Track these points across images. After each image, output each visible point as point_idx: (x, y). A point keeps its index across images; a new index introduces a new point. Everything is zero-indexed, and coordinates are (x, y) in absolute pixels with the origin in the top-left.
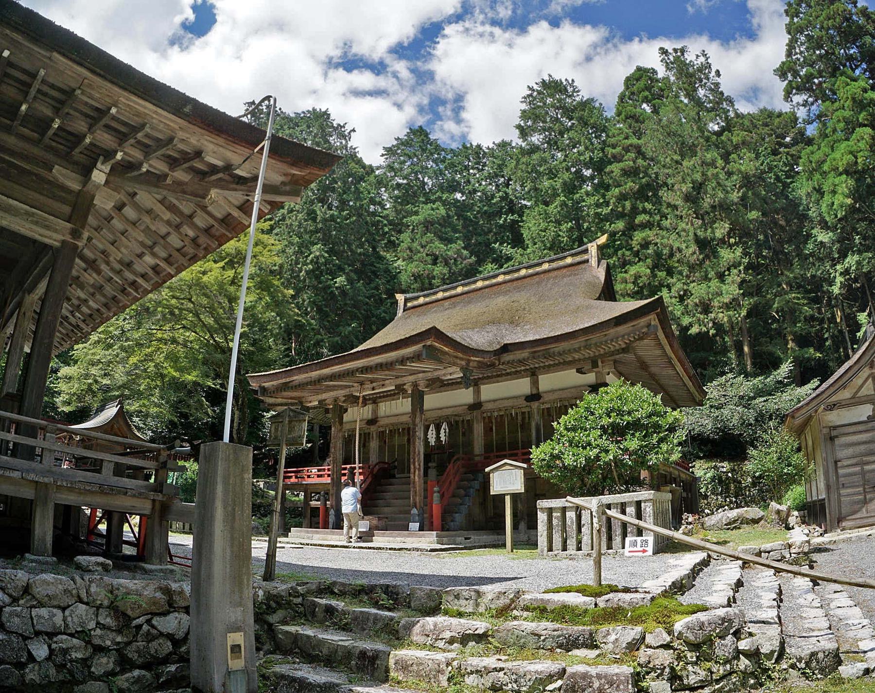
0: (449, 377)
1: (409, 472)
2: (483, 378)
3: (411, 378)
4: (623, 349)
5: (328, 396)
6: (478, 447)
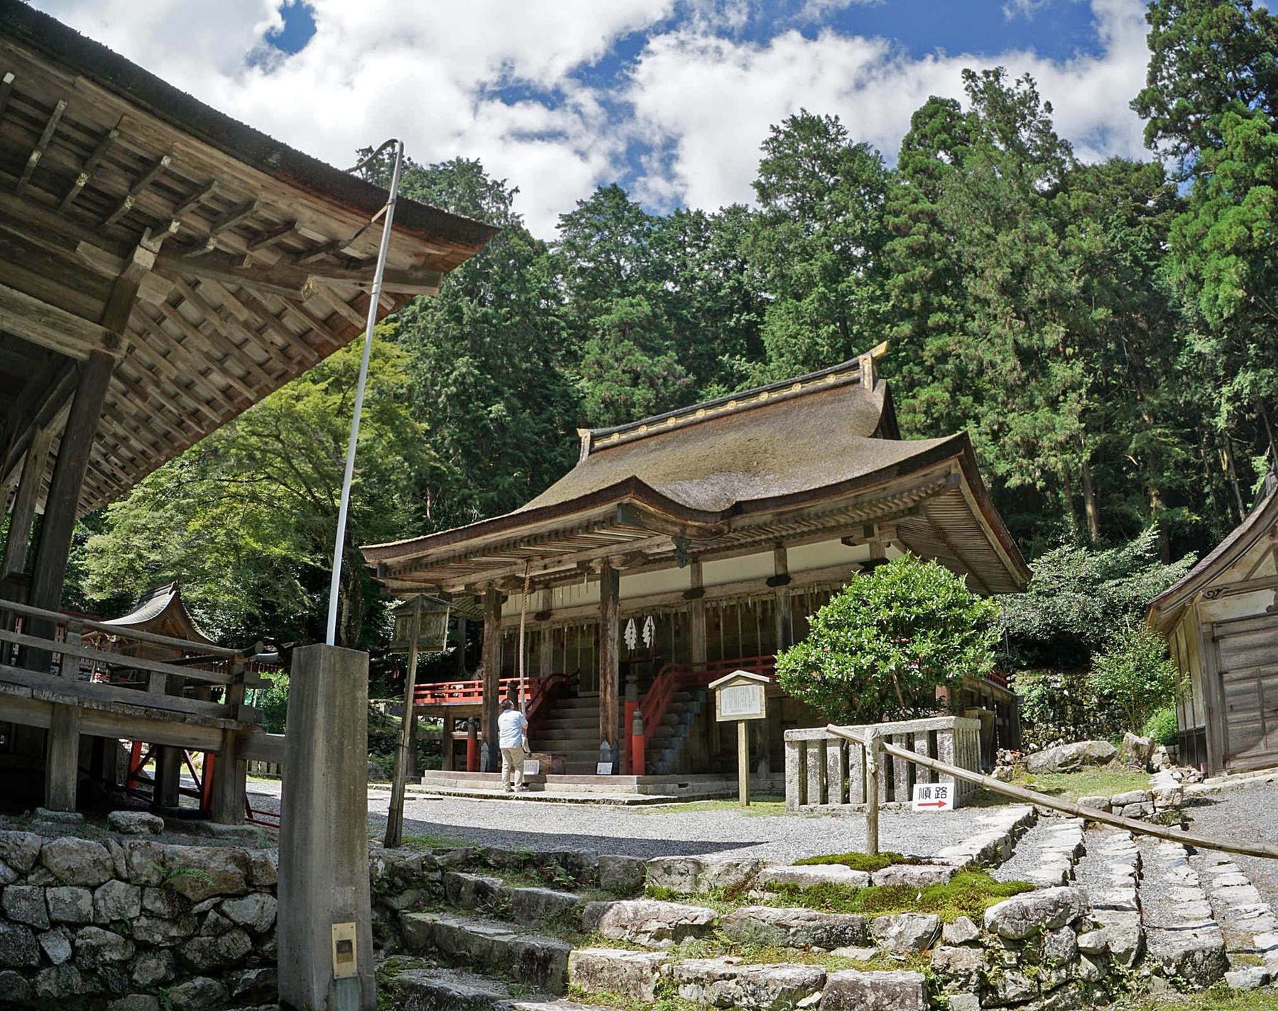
0: (656, 550)
1: (597, 688)
2: (706, 552)
3: (601, 552)
4: (910, 509)
5: (479, 578)
6: (699, 651)
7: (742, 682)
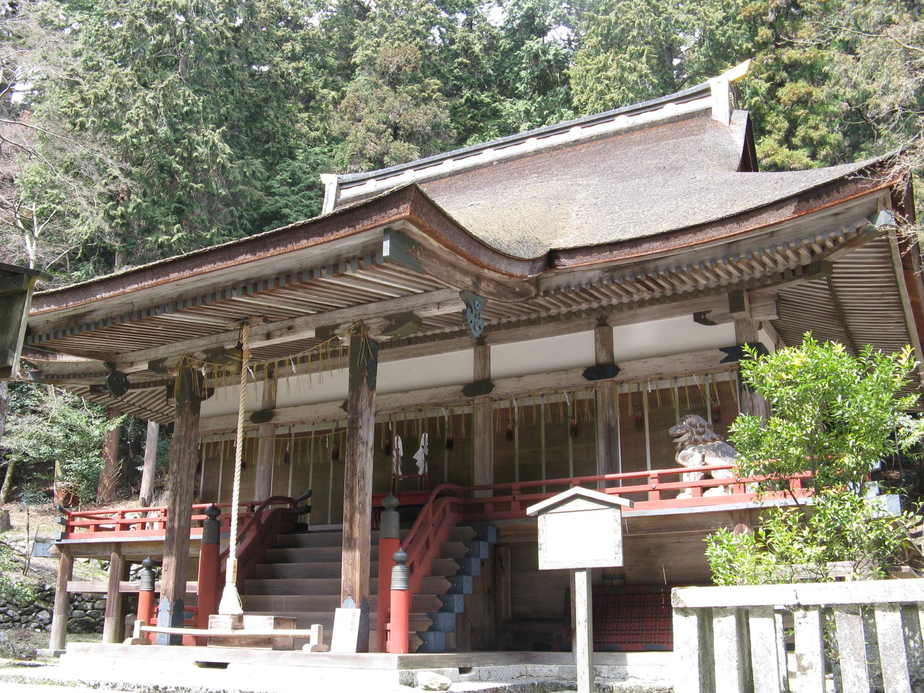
0: (435, 312)
1: (339, 519)
2: (499, 327)
3: (352, 314)
4: (805, 268)
5: (171, 352)
6: (483, 471)
7: (579, 503)
